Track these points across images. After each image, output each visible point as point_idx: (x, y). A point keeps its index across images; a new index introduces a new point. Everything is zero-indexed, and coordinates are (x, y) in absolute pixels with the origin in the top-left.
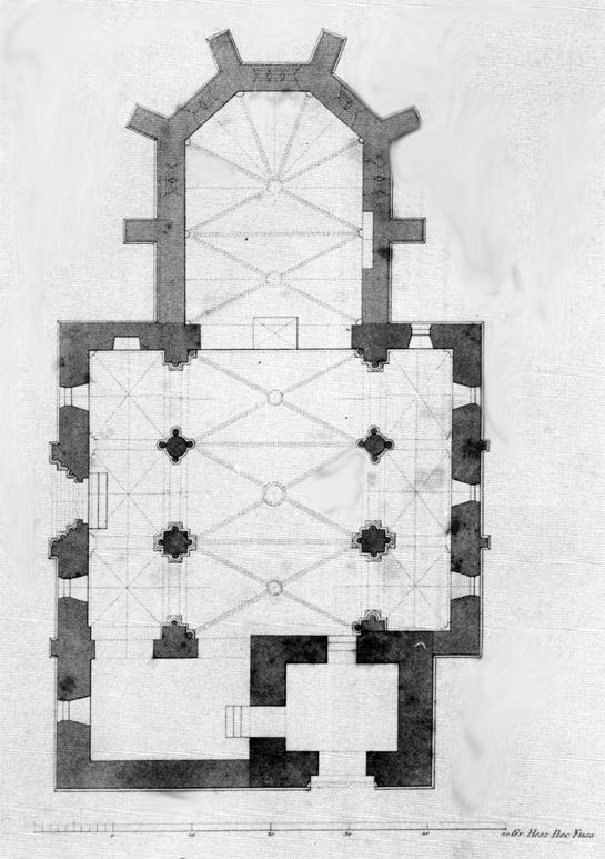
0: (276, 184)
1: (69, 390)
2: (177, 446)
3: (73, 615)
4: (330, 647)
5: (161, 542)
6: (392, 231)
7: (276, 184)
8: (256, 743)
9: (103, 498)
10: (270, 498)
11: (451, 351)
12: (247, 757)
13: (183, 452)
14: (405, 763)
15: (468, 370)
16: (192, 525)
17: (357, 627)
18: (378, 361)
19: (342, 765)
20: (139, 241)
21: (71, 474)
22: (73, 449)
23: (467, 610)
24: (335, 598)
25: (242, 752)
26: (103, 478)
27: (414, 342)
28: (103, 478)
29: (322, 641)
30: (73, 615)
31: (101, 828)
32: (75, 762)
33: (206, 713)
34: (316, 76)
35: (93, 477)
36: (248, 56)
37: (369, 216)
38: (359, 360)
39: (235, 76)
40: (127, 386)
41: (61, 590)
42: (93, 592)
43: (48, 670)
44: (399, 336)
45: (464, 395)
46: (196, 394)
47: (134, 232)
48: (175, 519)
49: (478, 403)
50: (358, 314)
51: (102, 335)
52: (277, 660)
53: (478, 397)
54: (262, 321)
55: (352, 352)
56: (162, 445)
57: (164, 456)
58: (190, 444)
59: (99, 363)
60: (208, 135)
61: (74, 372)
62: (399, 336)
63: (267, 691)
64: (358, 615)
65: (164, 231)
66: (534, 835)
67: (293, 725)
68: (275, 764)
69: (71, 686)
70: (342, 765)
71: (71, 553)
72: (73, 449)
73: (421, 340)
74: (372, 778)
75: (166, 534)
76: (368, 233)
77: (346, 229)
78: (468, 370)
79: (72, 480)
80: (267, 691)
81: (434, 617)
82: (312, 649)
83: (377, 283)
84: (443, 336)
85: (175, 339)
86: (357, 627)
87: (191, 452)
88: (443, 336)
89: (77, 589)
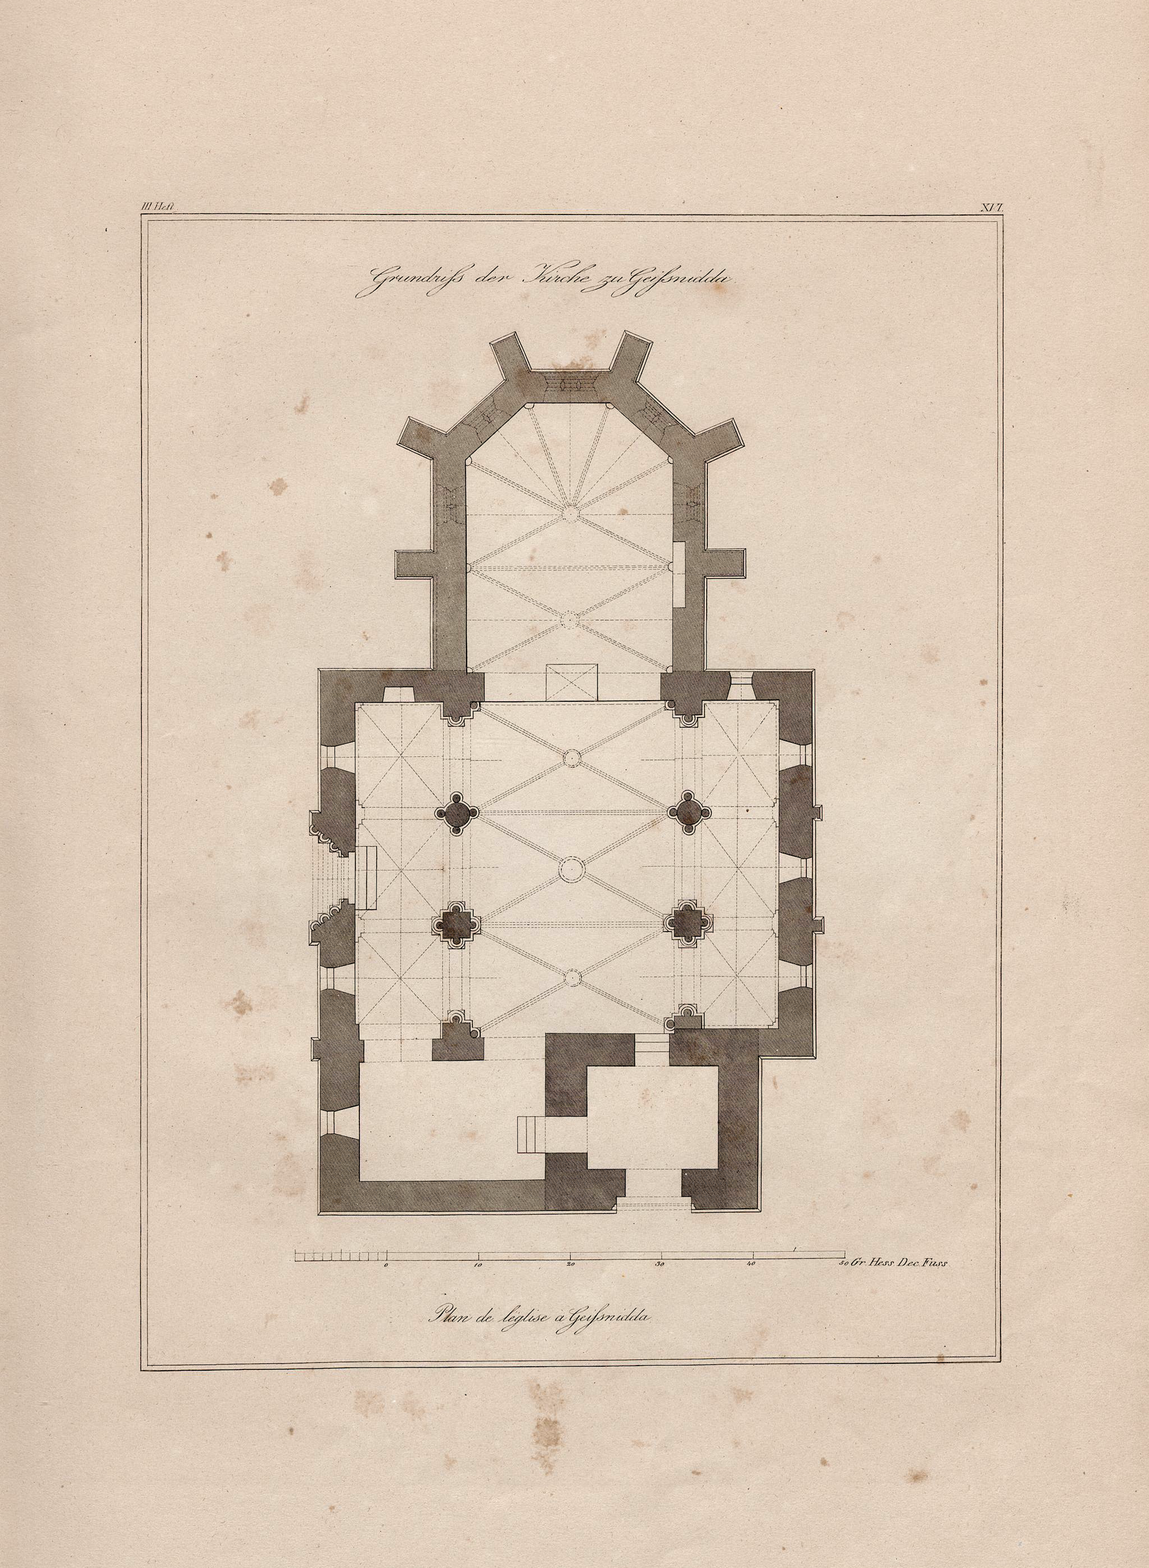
0: (568, 519)
1: (331, 749)
2: (458, 815)
3: (337, 1008)
4: (638, 1047)
5: (439, 925)
6: (712, 567)
7: (568, 519)
8: (553, 1160)
9: (372, 875)
10: (566, 873)
11: (777, 702)
12: (541, 1176)
13: (465, 822)
14: (724, 1183)
15: (797, 726)
16: (478, 907)
17: (670, 1024)
18: (690, 713)
19: (654, 1185)
20: (414, 576)
21: (335, 848)
22: (336, 818)
23: (798, 1005)
24: (647, 984)
25: (536, 1170)
26: (372, 851)
27: (734, 692)
28: (372, 851)
29: (628, 1040)
30: (337, 1008)
31: (373, 1257)
32: (341, 1182)
33: (494, 1119)
34: (616, 382)
35: (361, 851)
36: (538, 362)
37: (680, 547)
38: (670, 713)
39: (526, 384)
40: (398, 742)
41: (324, 981)
42: (362, 985)
43: (309, 1075)
44: (719, 685)
45: (792, 868)
46: (482, 754)
47: (408, 566)
48: (456, 897)
49: (809, 876)
50: (667, 660)
51: (375, 684)
52: (572, 1066)
53: (810, 870)
54: (558, 669)
55: (661, 704)
56: (441, 814)
57: (444, 827)
58: (473, 813)
59: (367, 716)
60: (490, 454)
61: (338, 728)
62: (719, 685)
63: (565, 1098)
64: (669, 1009)
65: (440, 566)
66: (878, 1264)
67: (593, 1137)
68: (577, 1185)
69: (340, 1086)
70: (654, 1185)
71: (336, 936)
72: (336, 818)
73: (742, 690)
74: (712, 708)
75: (446, 915)
76: (680, 566)
77: (655, 562)
78: (797, 726)
79: (336, 854)
80: (565, 1098)
81: (761, 1015)
82: (620, 1050)
83: (690, 624)
84: (768, 685)
85: (453, 688)
86: (670, 1024)
87: (474, 823)
88: (768, 685)
89: (342, 979)
